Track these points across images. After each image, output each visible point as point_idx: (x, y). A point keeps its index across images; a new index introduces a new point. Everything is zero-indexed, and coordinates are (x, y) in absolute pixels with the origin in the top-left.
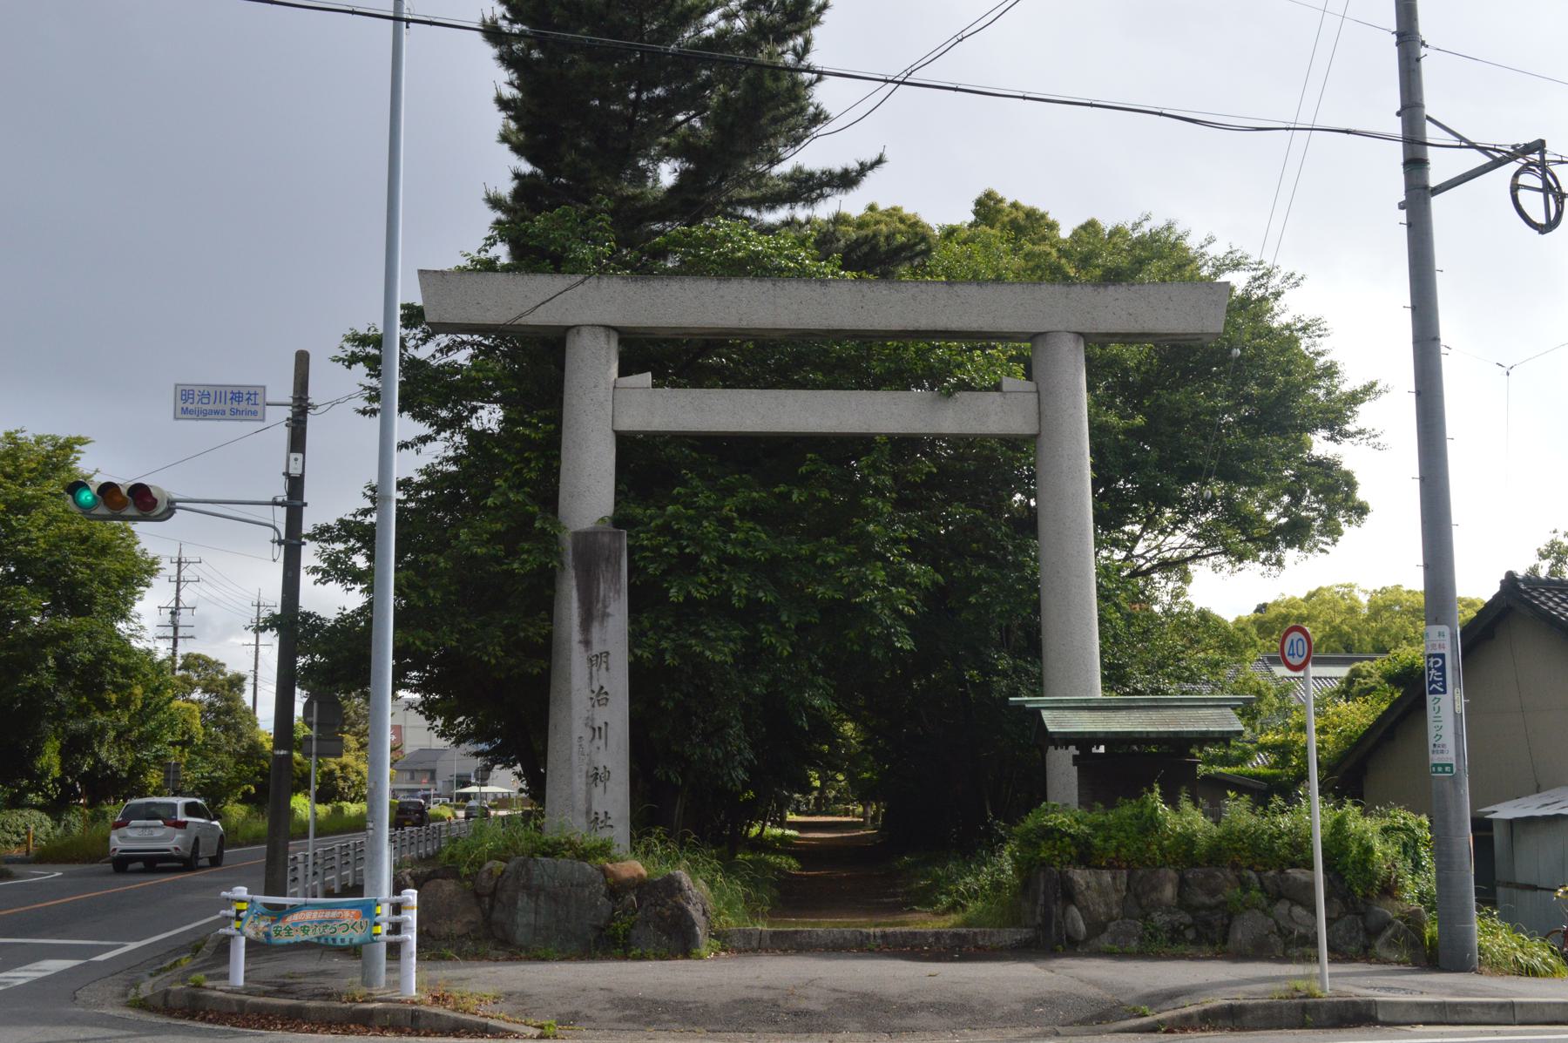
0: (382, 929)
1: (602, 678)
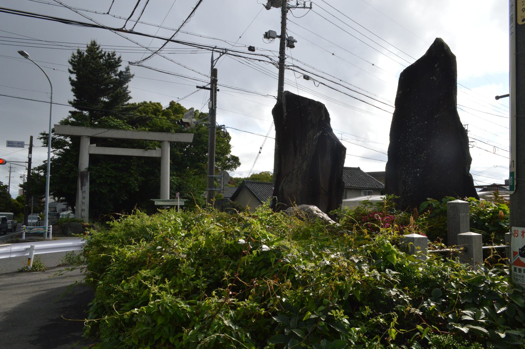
0: (47, 231)
1: (84, 195)
